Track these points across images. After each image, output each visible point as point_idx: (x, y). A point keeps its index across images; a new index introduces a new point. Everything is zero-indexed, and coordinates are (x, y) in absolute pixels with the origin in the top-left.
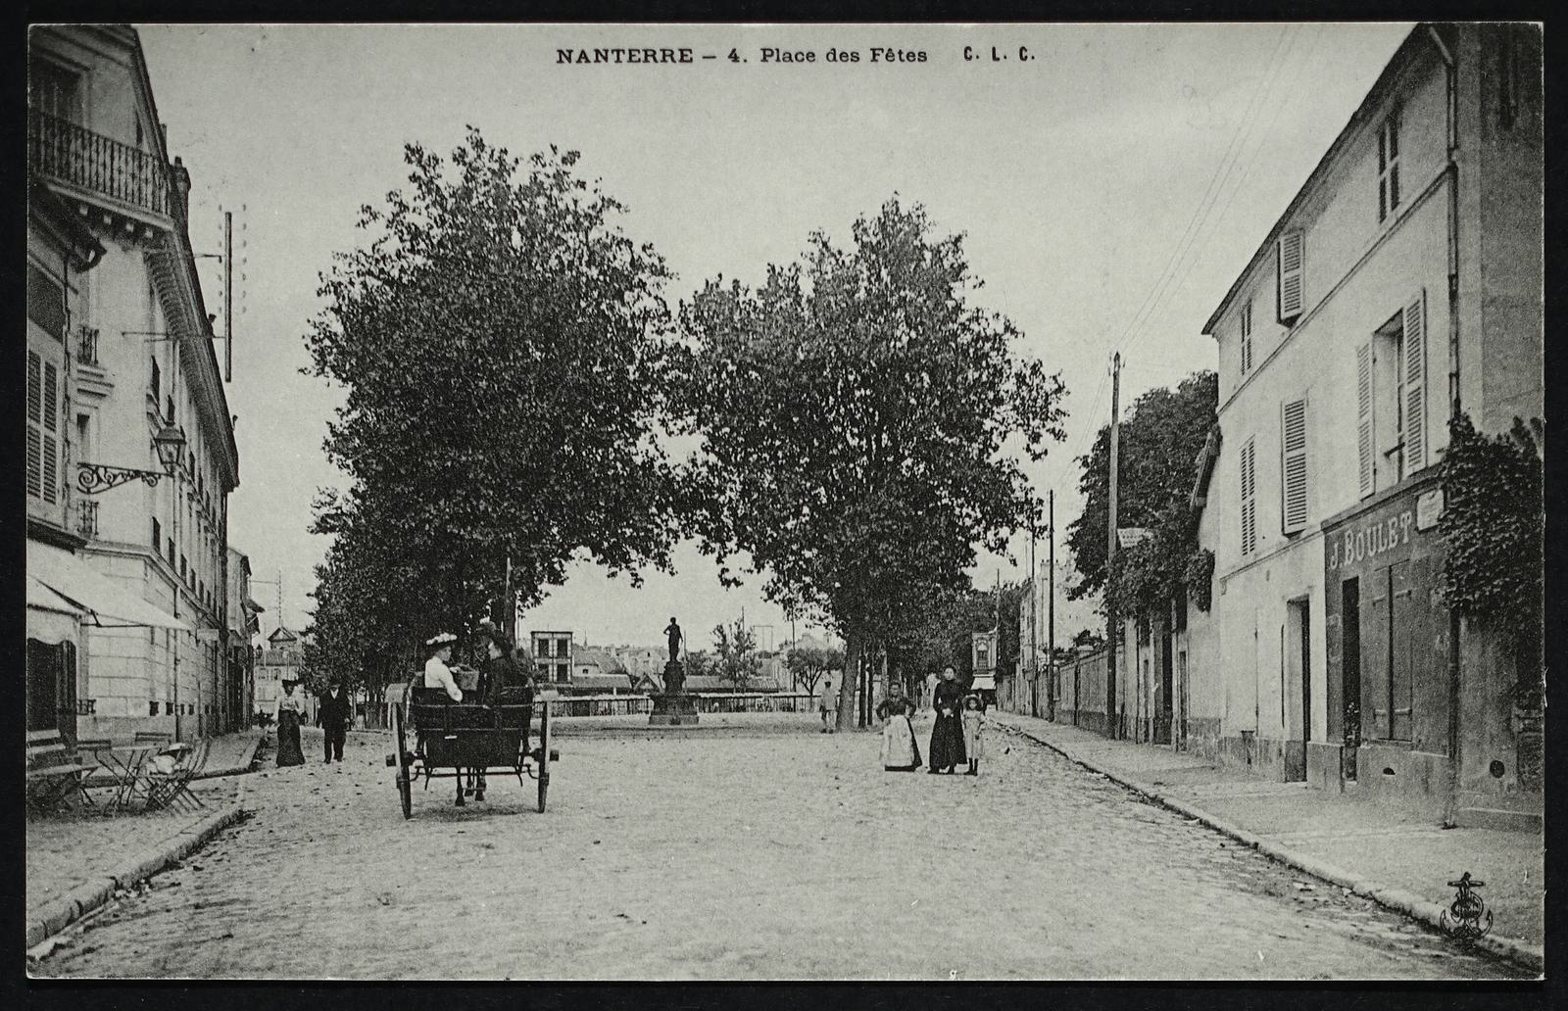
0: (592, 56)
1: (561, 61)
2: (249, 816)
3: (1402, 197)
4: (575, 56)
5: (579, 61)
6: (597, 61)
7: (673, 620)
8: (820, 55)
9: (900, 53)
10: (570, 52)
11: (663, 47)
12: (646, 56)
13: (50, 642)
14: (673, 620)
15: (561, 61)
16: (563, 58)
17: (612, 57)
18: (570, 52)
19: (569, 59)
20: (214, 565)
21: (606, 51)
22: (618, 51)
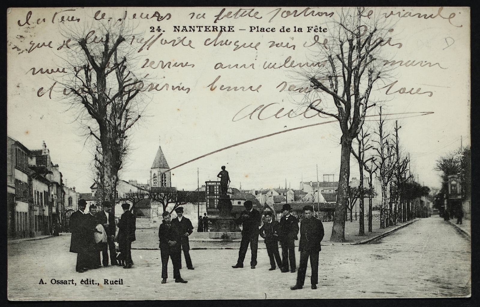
0: (188, 29)
1: (175, 31)
2: (138, 187)
3: (152, 35)
4: (181, 29)
5: (182, 31)
6: (190, 31)
7: (223, 168)
8: (277, 30)
9: (320, 28)
10: (179, 27)
11: (284, 33)
12: (214, 29)
13: (29, 149)
14: (223, 168)
15: (175, 31)
16: (176, 30)
17: (197, 29)
18: (179, 27)
19: (179, 30)
20: (405, 233)
21: (194, 27)
22: (200, 27)
